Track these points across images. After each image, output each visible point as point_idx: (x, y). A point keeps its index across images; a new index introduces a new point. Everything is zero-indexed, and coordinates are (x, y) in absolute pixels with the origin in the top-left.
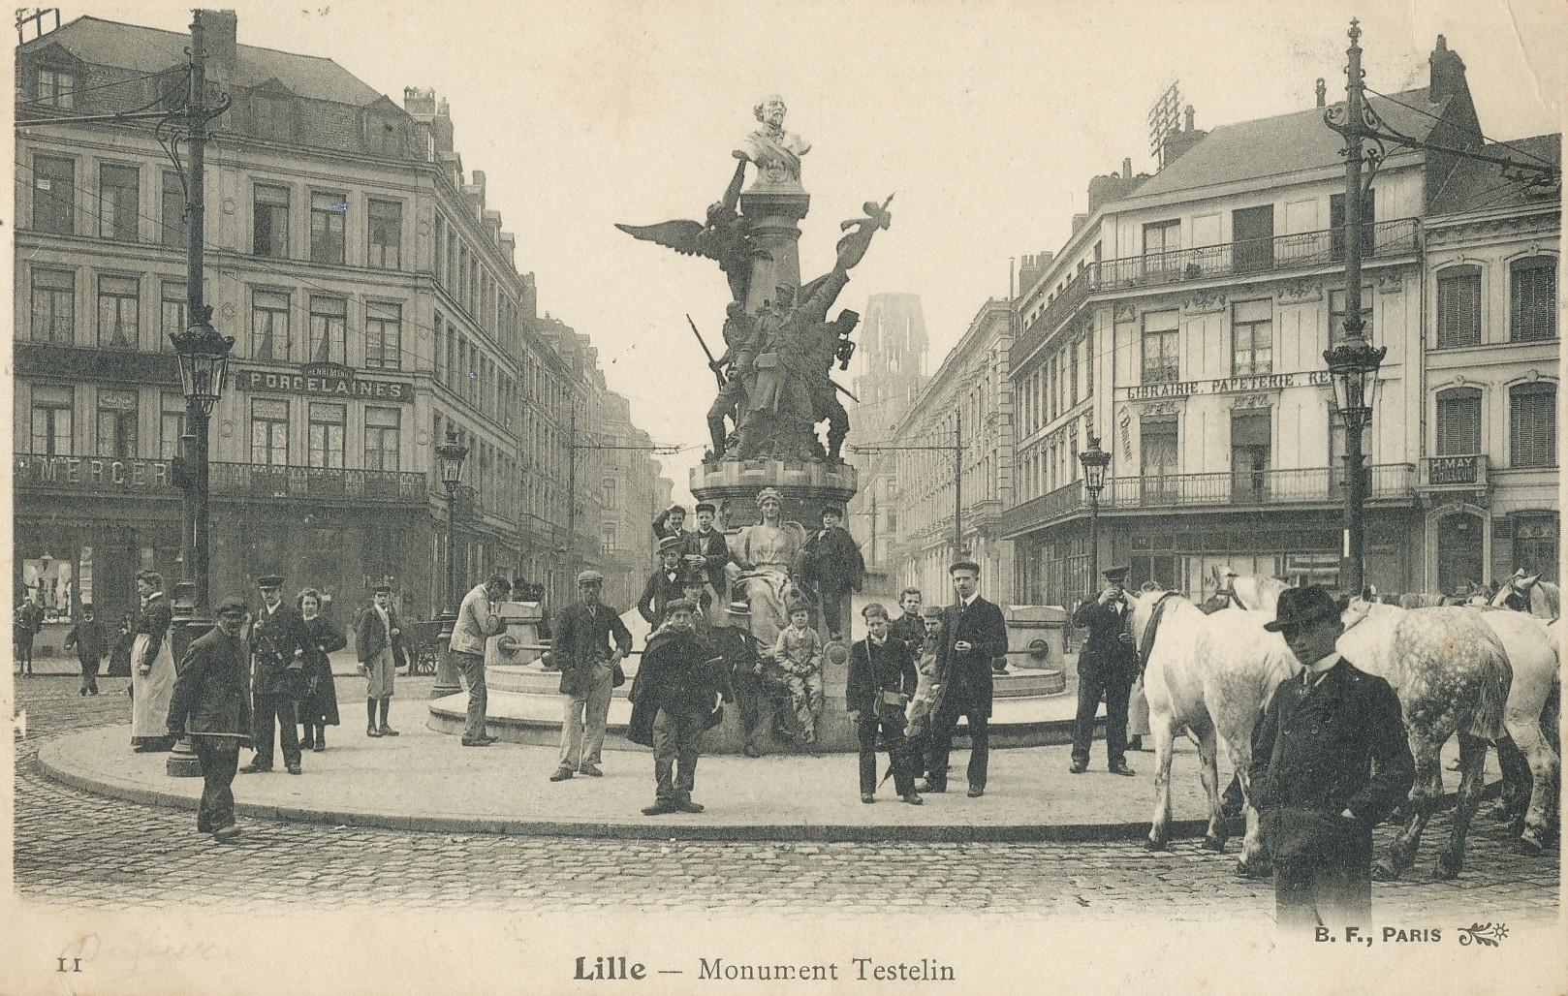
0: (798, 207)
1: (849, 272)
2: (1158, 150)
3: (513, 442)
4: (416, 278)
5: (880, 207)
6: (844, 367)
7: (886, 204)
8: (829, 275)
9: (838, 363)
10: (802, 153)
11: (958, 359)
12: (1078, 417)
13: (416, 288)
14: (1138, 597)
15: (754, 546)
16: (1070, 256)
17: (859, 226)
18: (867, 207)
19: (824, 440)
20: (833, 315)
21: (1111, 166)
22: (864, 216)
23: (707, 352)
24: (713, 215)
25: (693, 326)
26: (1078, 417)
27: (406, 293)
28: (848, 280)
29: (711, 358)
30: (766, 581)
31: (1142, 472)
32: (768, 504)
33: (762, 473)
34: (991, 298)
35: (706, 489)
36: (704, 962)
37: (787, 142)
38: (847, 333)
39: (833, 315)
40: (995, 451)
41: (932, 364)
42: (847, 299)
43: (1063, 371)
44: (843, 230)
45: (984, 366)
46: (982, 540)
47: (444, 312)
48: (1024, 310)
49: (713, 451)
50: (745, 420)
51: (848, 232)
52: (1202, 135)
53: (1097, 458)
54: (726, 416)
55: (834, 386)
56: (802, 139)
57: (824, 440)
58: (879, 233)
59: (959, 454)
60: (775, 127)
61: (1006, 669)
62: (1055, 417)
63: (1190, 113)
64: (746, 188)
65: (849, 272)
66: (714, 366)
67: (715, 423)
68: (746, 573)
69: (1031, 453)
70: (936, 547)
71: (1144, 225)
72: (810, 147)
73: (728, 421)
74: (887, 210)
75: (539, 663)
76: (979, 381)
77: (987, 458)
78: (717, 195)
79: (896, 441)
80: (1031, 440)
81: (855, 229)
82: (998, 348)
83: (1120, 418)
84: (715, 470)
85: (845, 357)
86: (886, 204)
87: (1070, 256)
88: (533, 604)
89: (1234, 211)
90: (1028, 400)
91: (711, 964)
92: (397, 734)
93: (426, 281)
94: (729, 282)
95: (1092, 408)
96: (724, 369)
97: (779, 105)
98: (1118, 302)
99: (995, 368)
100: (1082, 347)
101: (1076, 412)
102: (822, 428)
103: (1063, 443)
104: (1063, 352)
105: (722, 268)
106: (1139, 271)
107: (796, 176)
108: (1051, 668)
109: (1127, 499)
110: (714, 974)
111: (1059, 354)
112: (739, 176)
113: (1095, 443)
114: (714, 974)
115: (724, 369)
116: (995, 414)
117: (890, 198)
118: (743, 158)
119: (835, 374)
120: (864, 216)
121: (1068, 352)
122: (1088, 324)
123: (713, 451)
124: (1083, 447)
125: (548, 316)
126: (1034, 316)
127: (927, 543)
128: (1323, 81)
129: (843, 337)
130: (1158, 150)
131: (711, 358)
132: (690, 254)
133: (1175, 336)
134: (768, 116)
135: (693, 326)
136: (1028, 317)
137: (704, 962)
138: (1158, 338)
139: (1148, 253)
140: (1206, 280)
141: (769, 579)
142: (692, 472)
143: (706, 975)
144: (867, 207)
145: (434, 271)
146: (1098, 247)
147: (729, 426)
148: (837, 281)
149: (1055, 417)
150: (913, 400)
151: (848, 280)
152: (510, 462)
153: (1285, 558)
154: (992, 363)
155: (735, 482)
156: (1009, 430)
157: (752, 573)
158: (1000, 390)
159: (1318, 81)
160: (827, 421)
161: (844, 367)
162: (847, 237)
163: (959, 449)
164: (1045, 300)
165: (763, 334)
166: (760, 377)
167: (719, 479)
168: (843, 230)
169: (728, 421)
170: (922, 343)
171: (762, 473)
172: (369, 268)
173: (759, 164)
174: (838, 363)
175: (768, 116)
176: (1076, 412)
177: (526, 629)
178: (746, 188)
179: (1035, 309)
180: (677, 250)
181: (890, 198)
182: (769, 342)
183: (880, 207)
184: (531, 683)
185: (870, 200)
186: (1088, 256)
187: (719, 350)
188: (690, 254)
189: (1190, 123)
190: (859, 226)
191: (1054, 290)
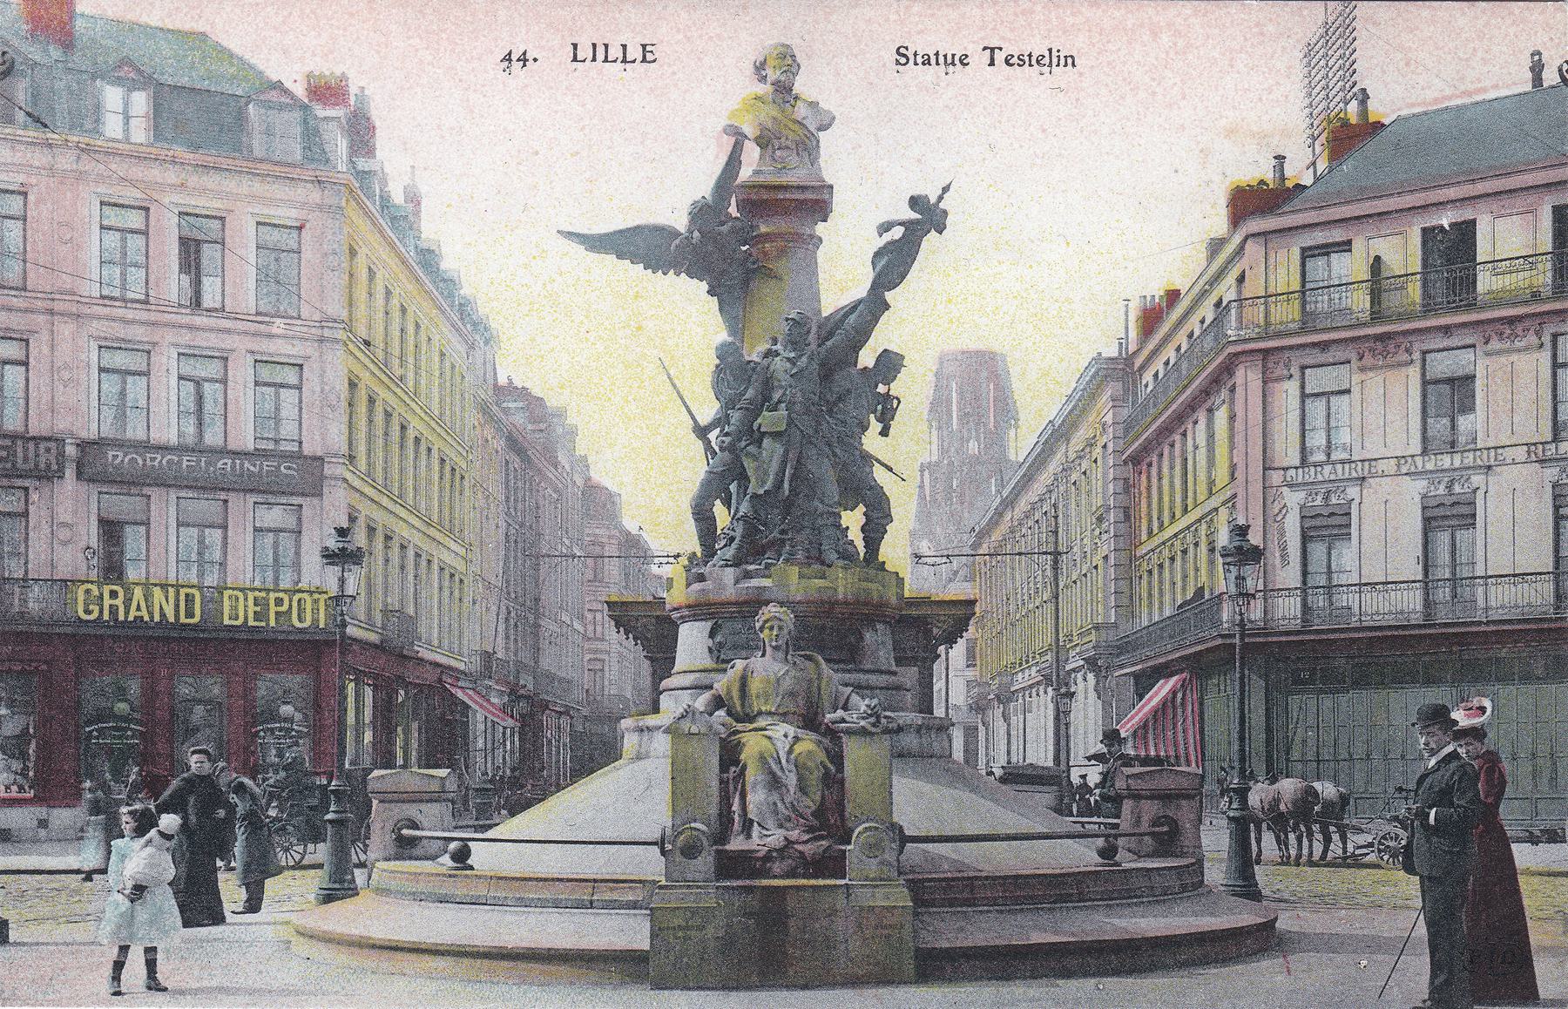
0: (816, 204)
1: (889, 296)
3: (462, 552)
4: (323, 327)
5: (933, 200)
6: (884, 433)
7: (940, 198)
8: (860, 302)
9: (875, 426)
10: (822, 128)
11: (1058, 434)
12: (1216, 509)
13: (321, 340)
14: (703, 197)
16: (1204, 294)
17: (902, 229)
18: (914, 202)
19: (856, 536)
21: (1258, 170)
24: (702, 213)
26: (1216, 509)
27: (310, 349)
28: (887, 307)
29: (693, 418)
32: (771, 628)
33: (767, 582)
34: (1100, 354)
39: (867, 358)
41: (1022, 443)
42: (885, 336)
43: (1196, 448)
45: (1091, 444)
46: (1090, 676)
47: (365, 375)
48: (1143, 368)
50: (743, 509)
51: (887, 237)
52: (1379, 126)
53: (1245, 554)
54: (718, 502)
55: (867, 459)
57: (856, 536)
58: (931, 240)
59: (1056, 562)
60: (784, 91)
61: (1117, 858)
62: (1185, 511)
63: (1364, 97)
64: (745, 174)
65: (889, 296)
66: (702, 432)
67: (703, 517)
70: (1031, 686)
71: (1303, 250)
72: (834, 118)
74: (942, 205)
76: (1085, 465)
78: (703, 188)
79: (976, 546)
80: (1156, 541)
81: (897, 232)
85: (886, 419)
86: (940, 198)
87: (1204, 294)
88: (443, 772)
89: (1424, 230)
90: (1149, 488)
92: (165, 989)
93: (325, 332)
94: (721, 310)
95: (1235, 496)
100: (1221, 416)
101: (1214, 502)
102: (853, 520)
103: (1196, 544)
104: (1196, 422)
105: (711, 292)
106: (1296, 313)
107: (814, 161)
108: (1182, 855)
111: (1190, 426)
112: (733, 162)
113: (1241, 531)
115: (713, 436)
117: (946, 189)
118: (739, 138)
119: (872, 441)
121: (1202, 425)
122: (1230, 384)
123: (699, 555)
124: (1223, 538)
126: (1156, 375)
127: (1021, 680)
128: (1539, 53)
129: (881, 389)
131: (693, 418)
133: (1345, 398)
134: (772, 75)
136: (1148, 377)
138: (1324, 400)
139: (1308, 286)
140: (1392, 322)
144: (914, 202)
145: (346, 320)
146: (1241, 279)
148: (874, 305)
149: (1185, 511)
150: (999, 492)
151: (887, 307)
152: (457, 579)
158: (1111, 477)
159: (1532, 55)
160: (861, 508)
161: (884, 433)
163: (1056, 554)
164: (1169, 353)
166: (766, 442)
170: (1006, 410)
171: (767, 582)
172: (258, 314)
173: (763, 142)
174: (875, 426)
176: (1214, 502)
177: (434, 809)
178: (745, 174)
179: (1158, 366)
181: (946, 189)
182: (776, 396)
183: (933, 200)
185: (916, 192)
186: (1227, 290)
189: (1364, 112)
190: (902, 229)
191: (1181, 339)
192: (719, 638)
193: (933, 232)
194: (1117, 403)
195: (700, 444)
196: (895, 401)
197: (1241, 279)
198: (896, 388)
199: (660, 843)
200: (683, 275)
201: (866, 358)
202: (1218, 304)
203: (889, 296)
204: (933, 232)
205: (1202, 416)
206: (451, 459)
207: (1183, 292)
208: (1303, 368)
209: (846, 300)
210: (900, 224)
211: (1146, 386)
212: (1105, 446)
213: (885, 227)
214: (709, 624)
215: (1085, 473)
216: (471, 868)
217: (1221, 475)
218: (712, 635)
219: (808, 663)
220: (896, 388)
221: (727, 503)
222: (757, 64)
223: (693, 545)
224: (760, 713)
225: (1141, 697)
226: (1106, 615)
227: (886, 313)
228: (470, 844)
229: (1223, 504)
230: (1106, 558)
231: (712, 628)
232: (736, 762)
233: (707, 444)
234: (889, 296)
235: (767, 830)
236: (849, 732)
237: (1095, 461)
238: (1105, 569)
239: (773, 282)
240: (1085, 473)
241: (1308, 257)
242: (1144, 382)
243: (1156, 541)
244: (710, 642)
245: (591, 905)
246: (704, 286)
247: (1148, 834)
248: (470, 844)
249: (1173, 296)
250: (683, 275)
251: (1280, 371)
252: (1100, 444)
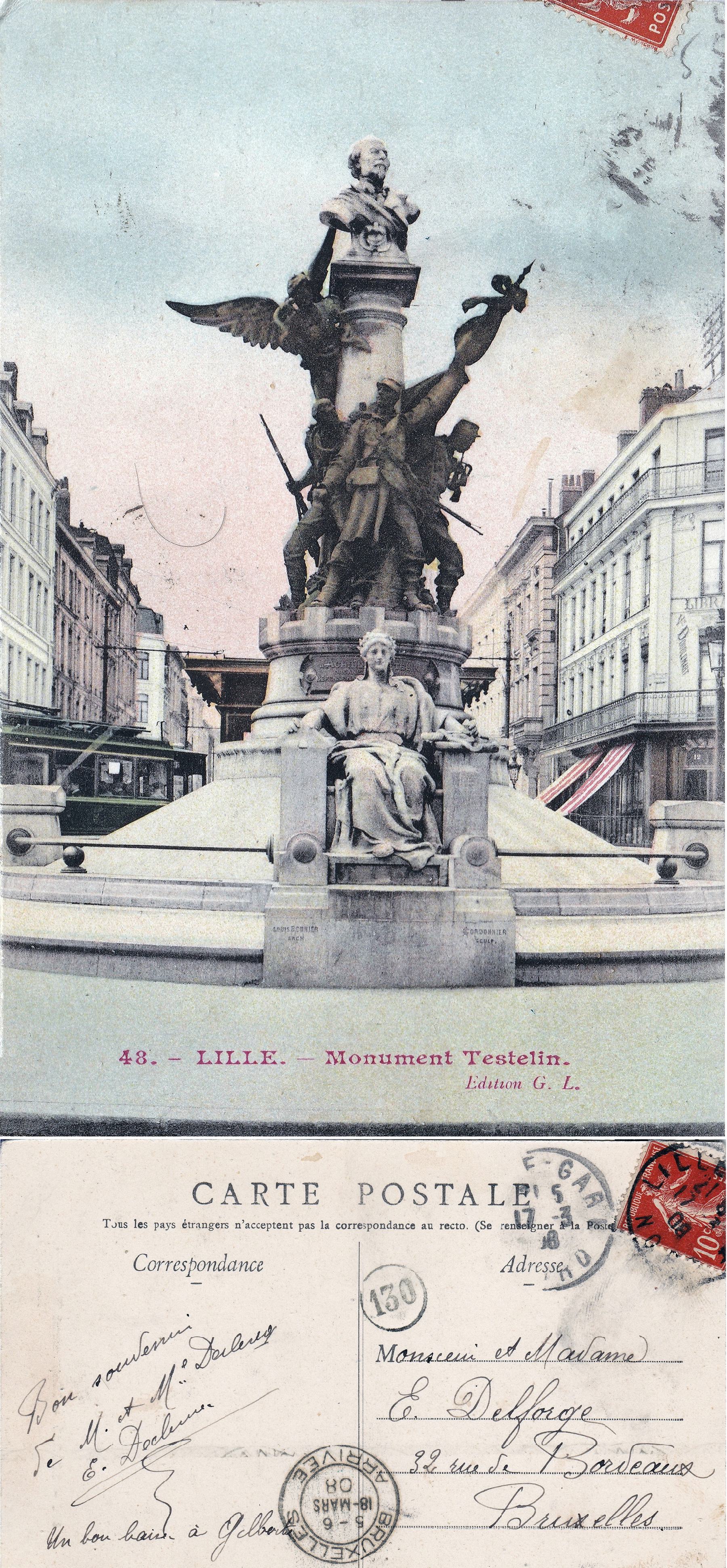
2: (712, 362)
5: (514, 280)
7: (521, 278)
19: (431, 586)
22: (491, 293)
25: (268, 432)
28: (467, 380)
30: (375, 755)
31: (700, 687)
36: (382, 1347)
37: (392, 201)
38: (463, 451)
40: (536, 669)
44: (465, 310)
49: (290, 595)
56: (408, 200)
57: (431, 586)
59: (508, 666)
66: (294, 487)
68: (344, 743)
69: (577, 670)
72: (419, 212)
73: (310, 561)
74: (522, 286)
77: (527, 677)
78: (303, 265)
80: (578, 656)
81: (480, 310)
82: (541, 564)
83: (678, 629)
84: (294, 618)
86: (521, 278)
91: (387, 1350)
96: (305, 492)
97: (382, 152)
98: (677, 509)
99: (537, 585)
100: (637, 559)
101: (630, 624)
102: (431, 571)
105: (304, 365)
109: (684, 713)
110: (389, 1358)
114: (389, 1358)
115: (305, 492)
116: (536, 631)
117: (527, 270)
118: (334, 223)
120: (491, 293)
130: (712, 362)
132: (263, 347)
135: (268, 432)
137: (382, 1347)
142: (263, 624)
143: (381, 1358)
144: (498, 281)
146: (657, 454)
155: (321, 633)
156: (551, 647)
160: (436, 562)
165: (361, 445)
167: (299, 629)
168: (465, 310)
169: (310, 561)
175: (366, 168)
180: (246, 341)
183: (514, 280)
187: (300, 466)
188: (263, 347)
193: (513, 311)
194: (547, 552)
195: (292, 498)
196: (468, 469)
197: (657, 454)
198: (469, 457)
199: (269, 852)
200: (279, 349)
201: (445, 427)
202: (636, 474)
203: (471, 370)
204: (513, 311)
205: (619, 557)
207: (598, 473)
208: (704, 522)
209: (429, 372)
211: (573, 539)
212: (537, 585)
213: (467, 305)
215: (519, 606)
216: (85, 871)
217: (636, 604)
218: (303, 668)
220: (469, 457)
221: (315, 555)
224: (363, 732)
225: (560, 774)
228: (84, 849)
229: (637, 626)
230: (536, 669)
231: (304, 662)
233: (299, 498)
234: (471, 370)
236: (444, 751)
237: (529, 597)
238: (535, 678)
239: (362, 354)
240: (519, 606)
241: (710, 438)
242: (571, 536)
243: (578, 656)
244: (301, 675)
245: (201, 907)
246: (298, 359)
248: (84, 849)
249: (589, 478)
250: (279, 349)
251: (686, 523)
252: (533, 582)
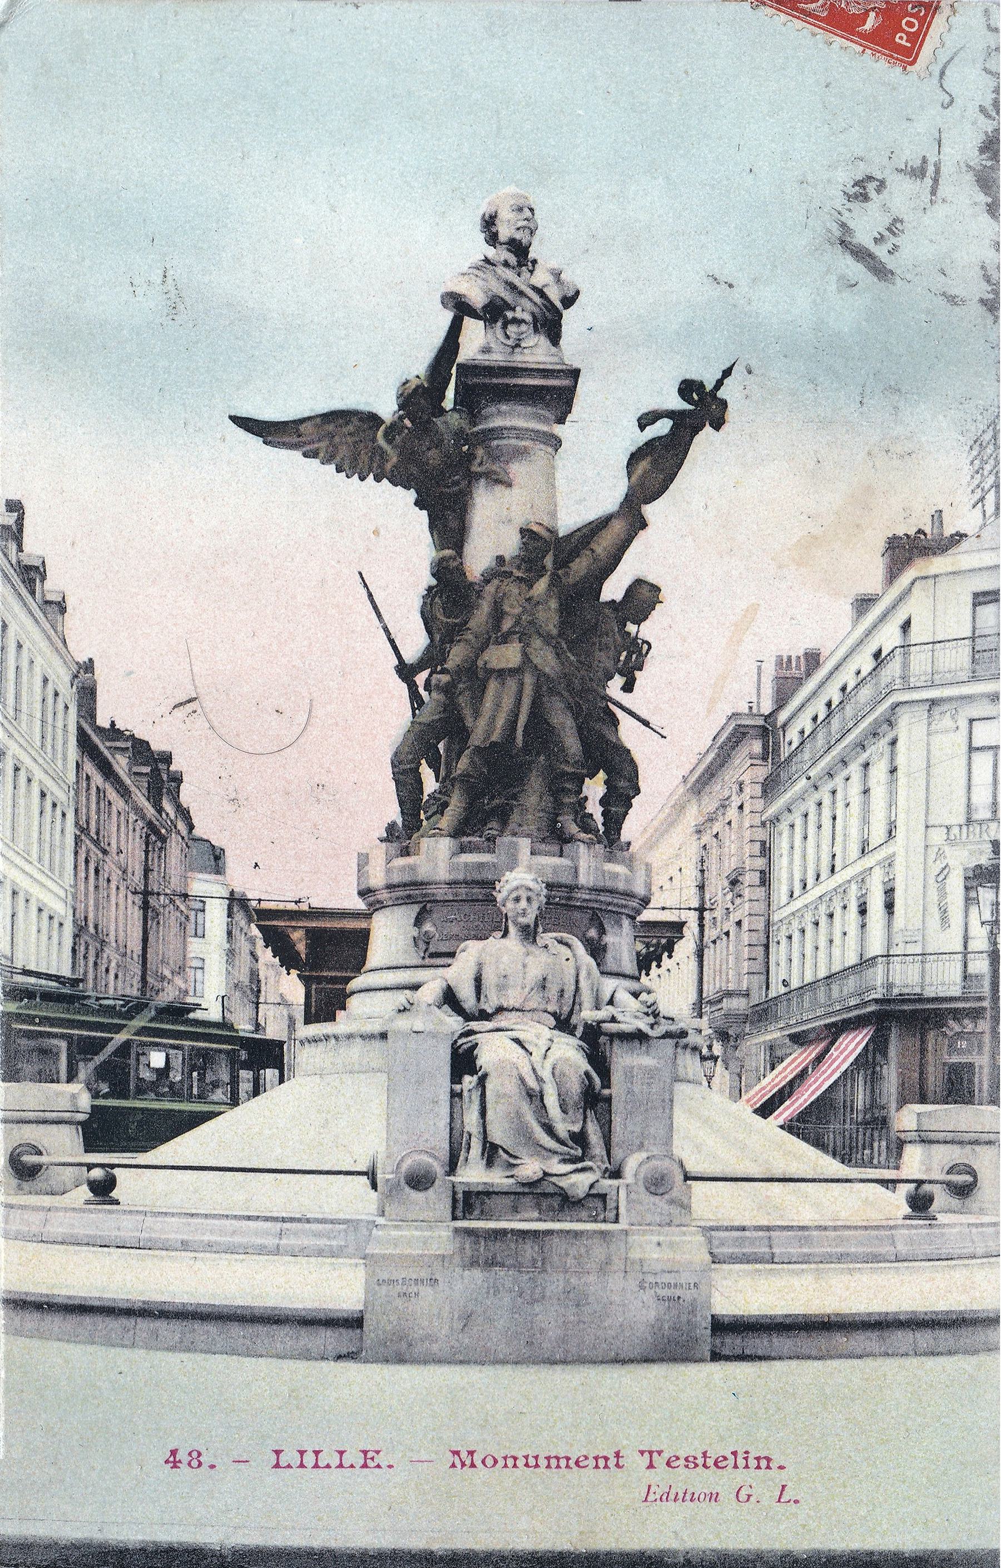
2: (982, 499)
5: (709, 387)
7: (719, 384)
15: (490, 979)
19: (594, 809)
20: (613, 589)
23: (173, 1168)
25: (370, 595)
28: (644, 525)
30: (517, 1041)
31: (966, 948)
32: (517, 900)
35: (390, 887)
37: (541, 278)
38: (638, 622)
39: (613, 589)
40: (739, 923)
44: (642, 427)
49: (399, 822)
57: (594, 809)
59: (701, 918)
60: (520, 250)
66: (406, 672)
68: (474, 1025)
71: (976, 595)
72: (577, 293)
74: (720, 394)
75: (84, 1193)
76: (717, 827)
77: (727, 934)
80: (798, 904)
81: (663, 427)
82: (746, 778)
84: (406, 852)
86: (719, 384)
96: (421, 678)
97: (526, 210)
98: (933, 703)
99: (741, 807)
100: (879, 772)
101: (869, 861)
102: (595, 788)
105: (419, 504)
109: (943, 984)
115: (421, 678)
117: (727, 373)
120: (676, 403)
125: (113, 724)
130: (982, 499)
132: (362, 479)
135: (370, 595)
141: (521, 1036)
142: (363, 861)
144: (688, 388)
146: (906, 626)
147: (430, 783)
153: (865, 1129)
154: (736, 801)
155: (443, 874)
156: (760, 893)
157: (489, 1025)
160: (602, 775)
162: (650, 444)
167: (412, 868)
168: (642, 427)
175: (505, 232)
177: (66, 1130)
180: (339, 470)
181: (727, 373)
183: (709, 387)
184: (60, 1225)
185: (693, 375)
192: (428, 927)
193: (708, 429)
196: (645, 647)
197: (906, 626)
199: (371, 1175)
200: (385, 481)
202: (877, 655)
203: (649, 511)
204: (708, 429)
205: (854, 769)
206: (52, 793)
208: (971, 721)
209: (592, 514)
210: (667, 416)
211: (790, 744)
212: (741, 807)
213: (645, 421)
214: (416, 908)
216: (117, 1202)
218: (418, 922)
219: (563, 949)
220: (647, 630)
222: (487, 216)
223: (393, 813)
224: (500, 1010)
225: (773, 1068)
226: (740, 981)
227: (642, 533)
228: (116, 1171)
230: (739, 923)
231: (419, 914)
232: (473, 1070)
234: (649, 511)
235: (516, 1157)
236: (612, 1036)
237: (729, 823)
238: (738, 936)
239: (499, 489)
241: (980, 604)
242: (787, 740)
243: (798, 904)
244: (415, 932)
245: (277, 1251)
246: (411, 495)
247: (942, 1183)
248: (116, 1171)
250: (385, 481)
